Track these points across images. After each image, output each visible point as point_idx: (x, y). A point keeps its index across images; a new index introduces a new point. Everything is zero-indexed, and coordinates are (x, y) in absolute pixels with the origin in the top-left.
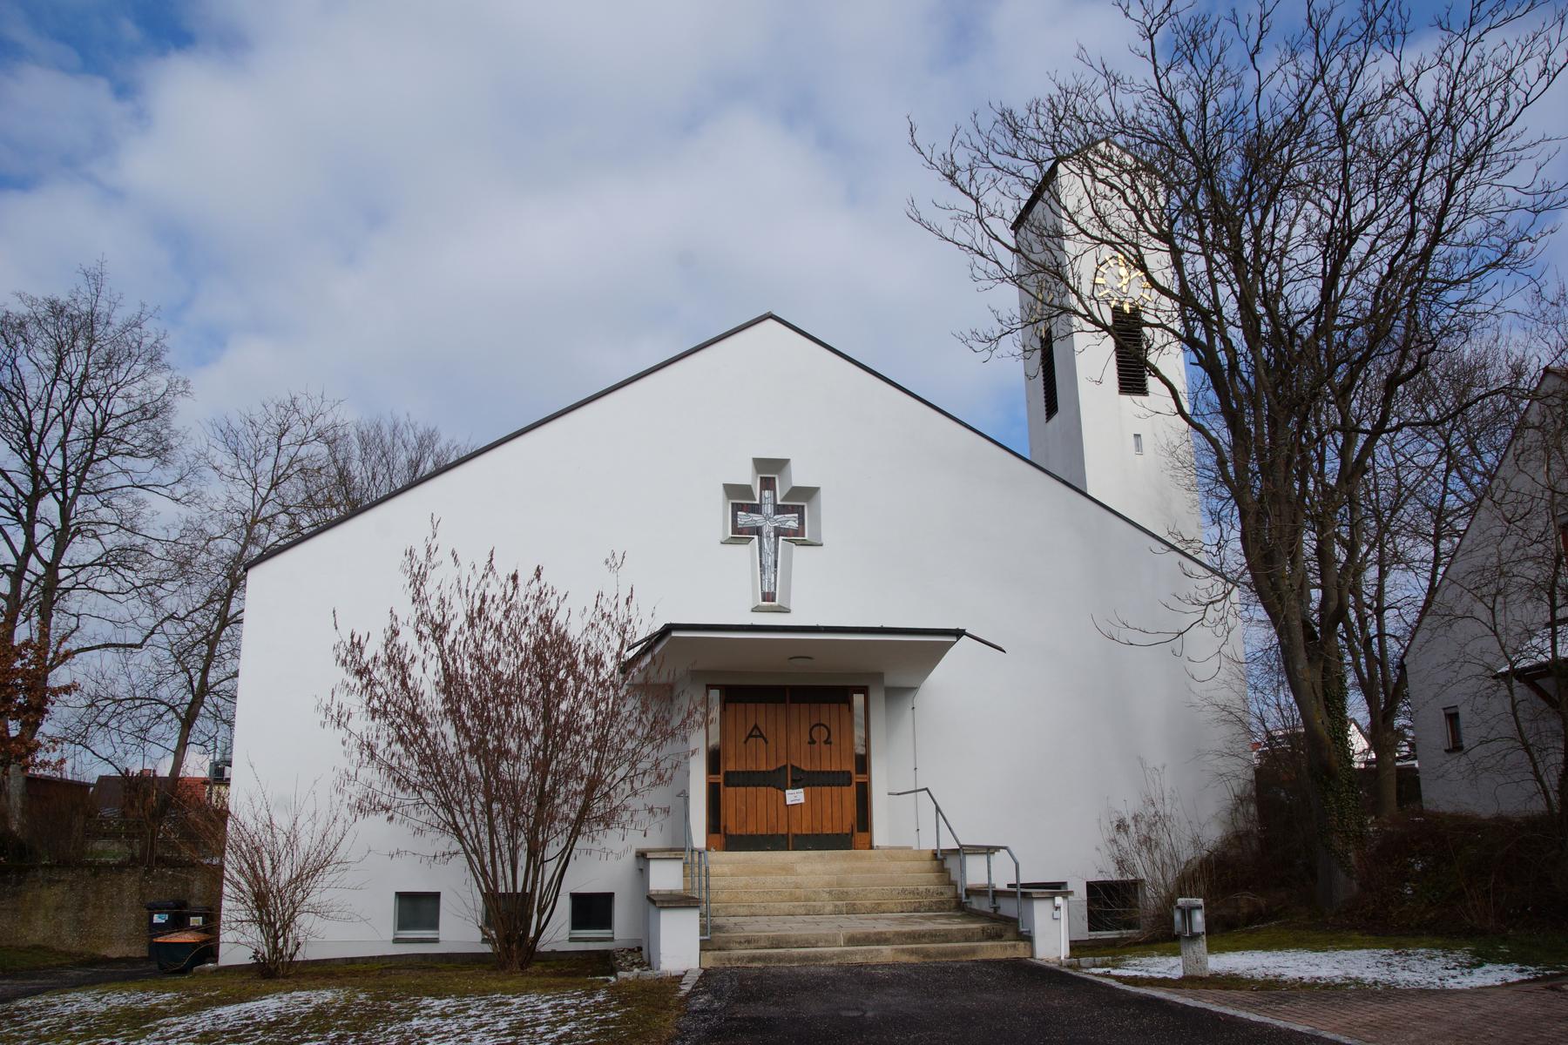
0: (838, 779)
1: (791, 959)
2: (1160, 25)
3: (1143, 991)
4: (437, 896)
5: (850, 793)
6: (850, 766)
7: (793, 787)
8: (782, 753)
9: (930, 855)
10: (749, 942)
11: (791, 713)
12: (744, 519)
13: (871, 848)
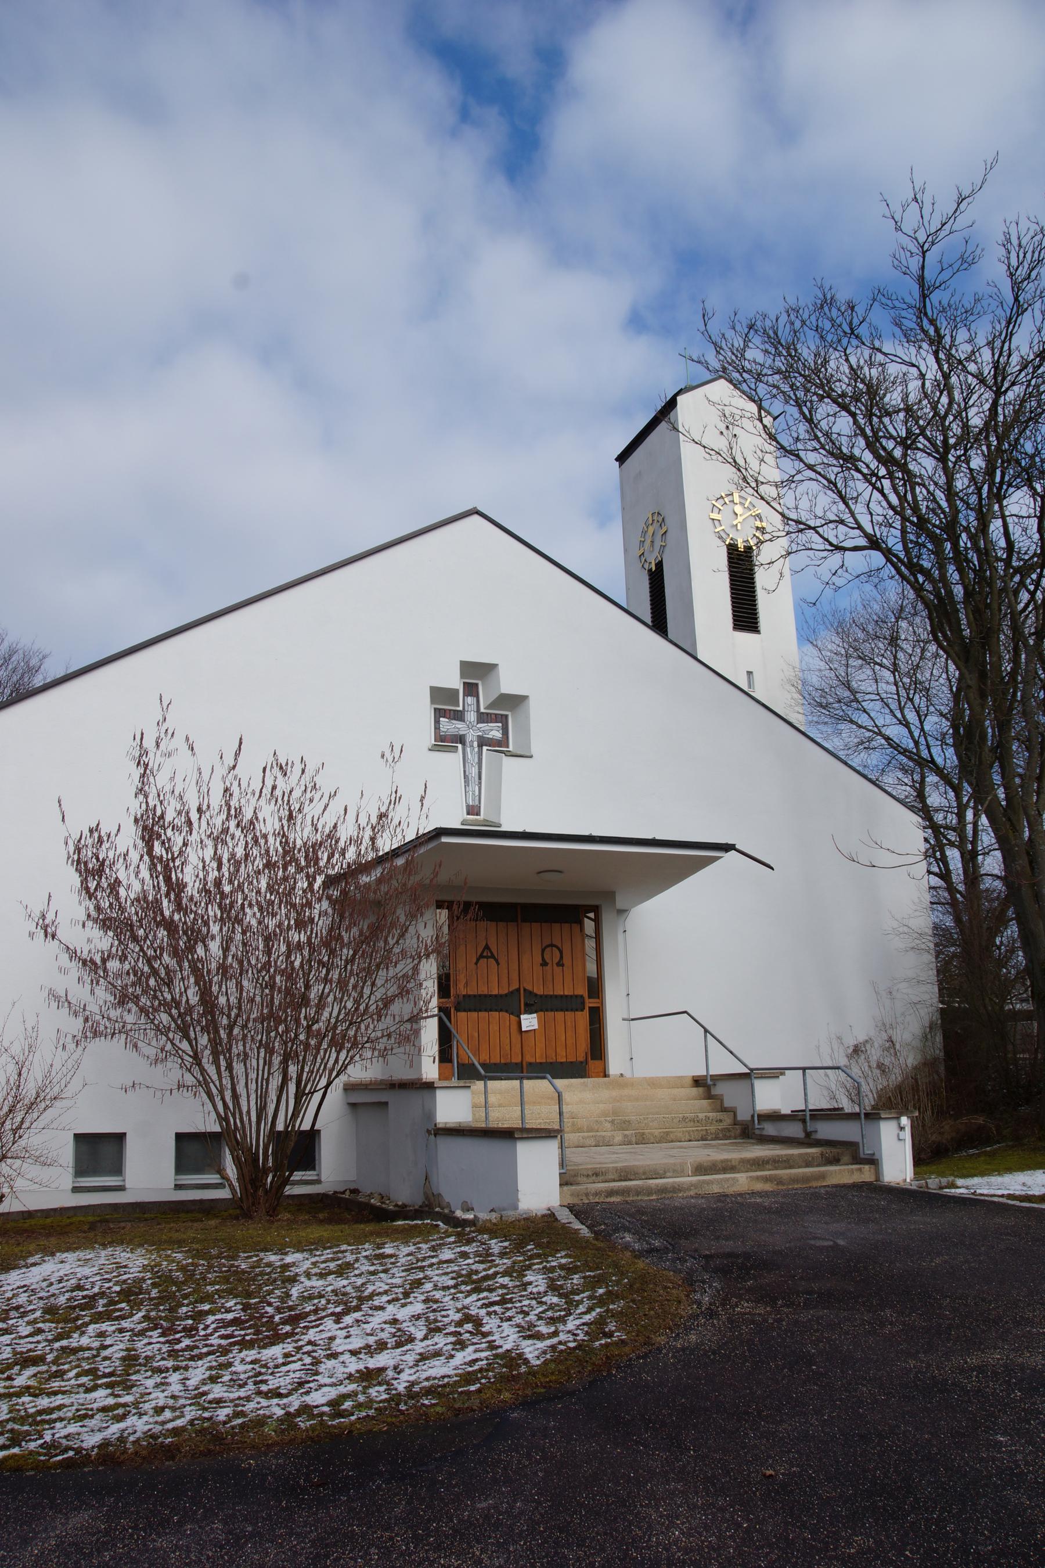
0: (569, 1003)
1: (649, 1191)
2: (933, 243)
3: (1017, 1203)
4: (120, 1137)
5: (583, 1018)
6: (582, 990)
8: (514, 976)
9: (690, 1082)
10: (596, 1174)
11: (519, 929)
12: (448, 726)
13: (605, 1076)
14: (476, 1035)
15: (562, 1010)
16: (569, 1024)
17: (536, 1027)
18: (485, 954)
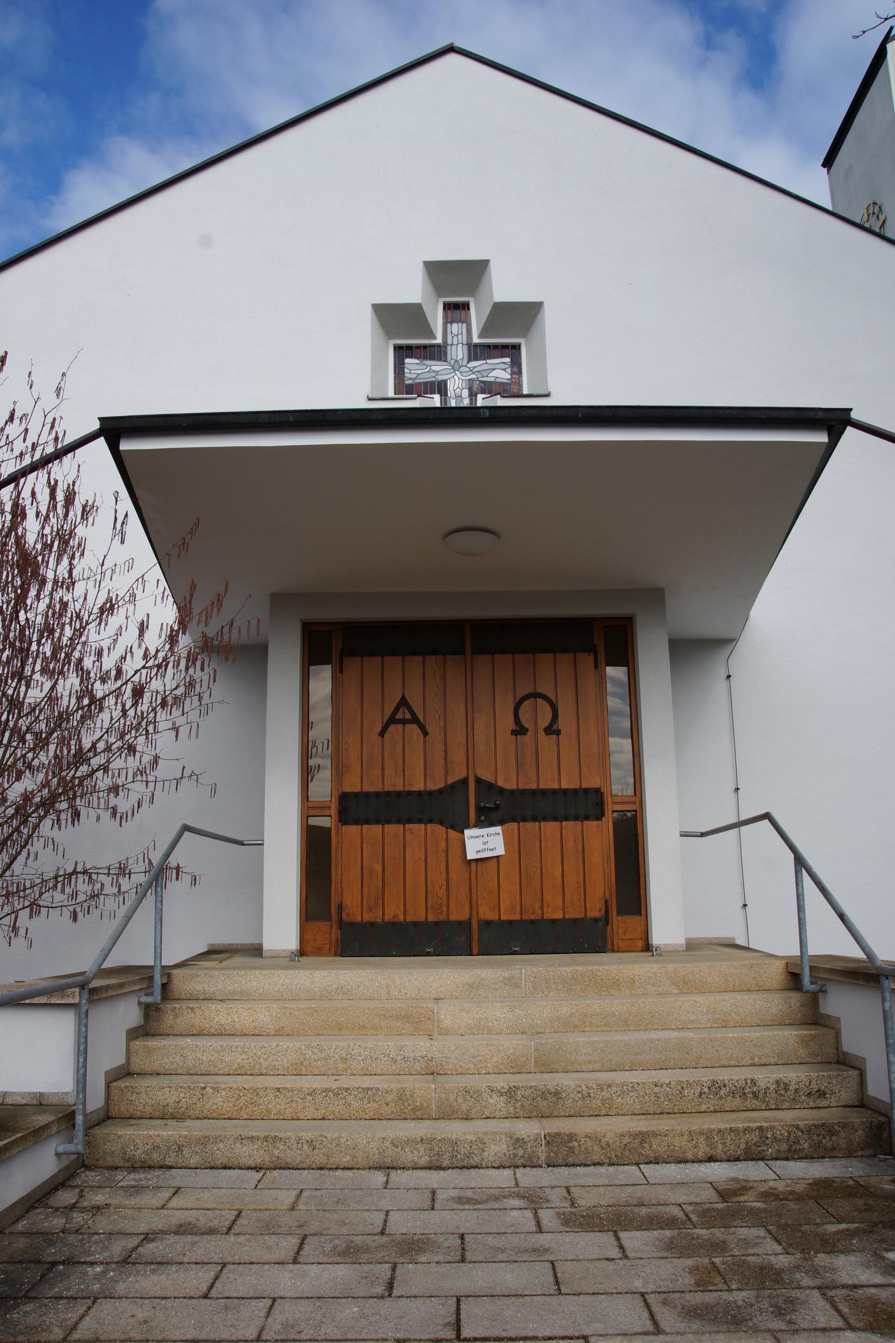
5: (600, 836)
7: (479, 824)
8: (458, 755)
9: (775, 973)
14: (378, 867)
15: (555, 819)
16: (570, 845)
17: (500, 851)
18: (399, 716)
